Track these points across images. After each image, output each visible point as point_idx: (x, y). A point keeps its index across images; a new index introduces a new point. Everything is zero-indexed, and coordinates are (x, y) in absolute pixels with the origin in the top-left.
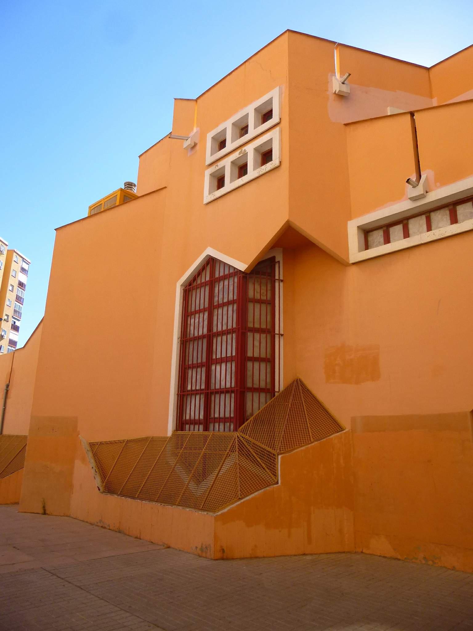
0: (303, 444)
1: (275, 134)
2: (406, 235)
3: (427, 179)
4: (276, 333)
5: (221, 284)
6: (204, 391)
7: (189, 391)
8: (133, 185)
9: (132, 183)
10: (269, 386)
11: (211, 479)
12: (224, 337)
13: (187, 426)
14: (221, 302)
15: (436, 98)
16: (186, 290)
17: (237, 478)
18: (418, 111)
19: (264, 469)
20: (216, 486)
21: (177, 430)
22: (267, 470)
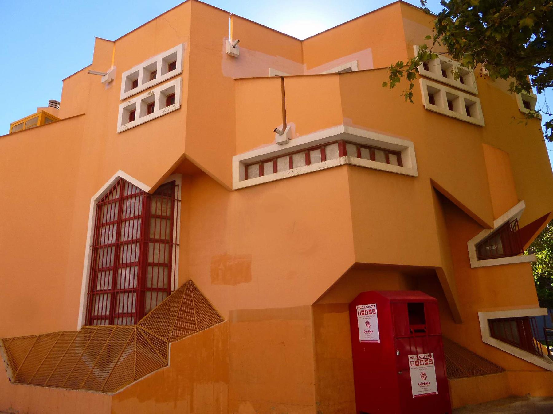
0: (190, 333)
1: (177, 82)
2: (275, 170)
3: (290, 129)
4: (173, 243)
5: (129, 201)
6: (111, 291)
7: (98, 291)
8: (58, 103)
9: (57, 102)
10: (165, 287)
11: (112, 365)
12: (130, 246)
13: (95, 321)
14: (128, 216)
15: (306, 64)
16: (99, 205)
17: (134, 362)
18: (286, 77)
19: (156, 353)
20: (116, 369)
21: (86, 324)
22: (160, 355)
